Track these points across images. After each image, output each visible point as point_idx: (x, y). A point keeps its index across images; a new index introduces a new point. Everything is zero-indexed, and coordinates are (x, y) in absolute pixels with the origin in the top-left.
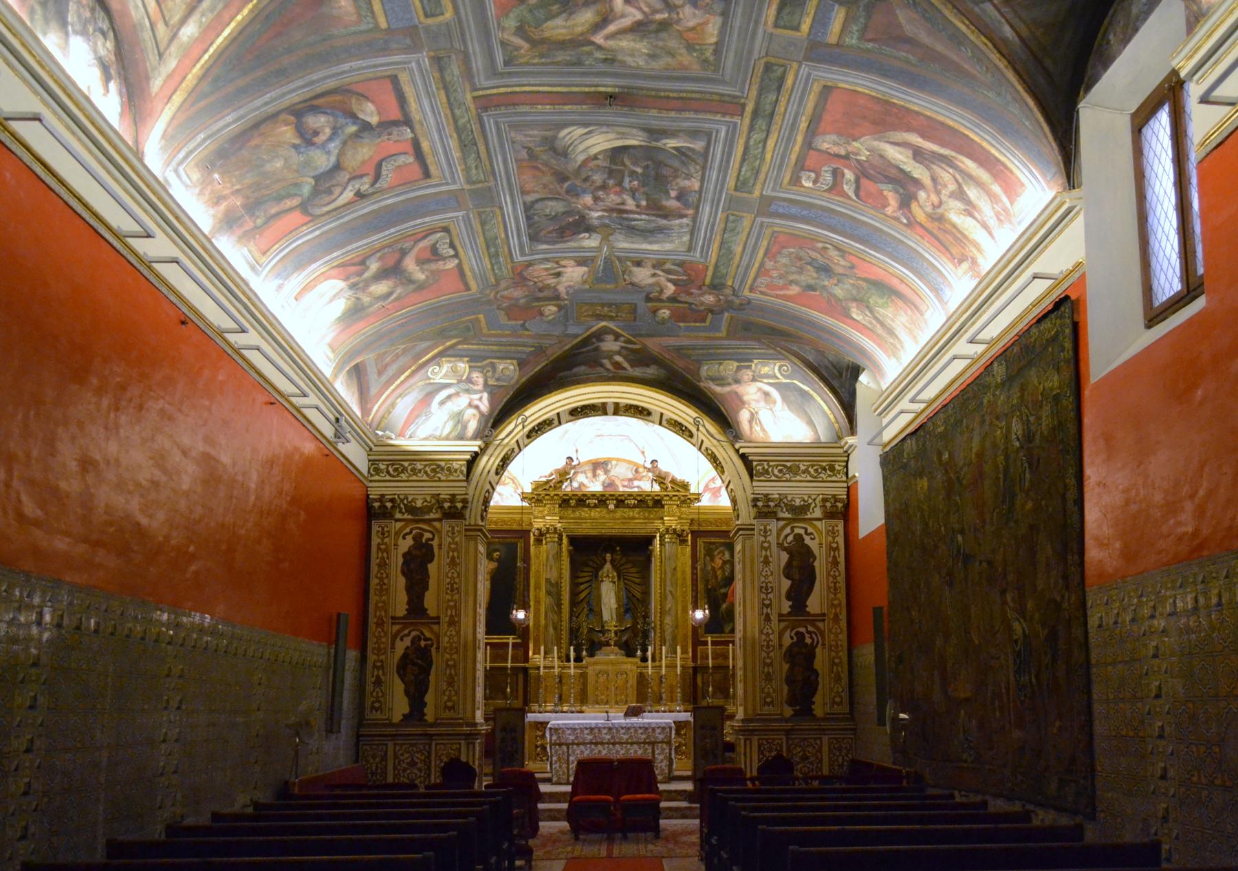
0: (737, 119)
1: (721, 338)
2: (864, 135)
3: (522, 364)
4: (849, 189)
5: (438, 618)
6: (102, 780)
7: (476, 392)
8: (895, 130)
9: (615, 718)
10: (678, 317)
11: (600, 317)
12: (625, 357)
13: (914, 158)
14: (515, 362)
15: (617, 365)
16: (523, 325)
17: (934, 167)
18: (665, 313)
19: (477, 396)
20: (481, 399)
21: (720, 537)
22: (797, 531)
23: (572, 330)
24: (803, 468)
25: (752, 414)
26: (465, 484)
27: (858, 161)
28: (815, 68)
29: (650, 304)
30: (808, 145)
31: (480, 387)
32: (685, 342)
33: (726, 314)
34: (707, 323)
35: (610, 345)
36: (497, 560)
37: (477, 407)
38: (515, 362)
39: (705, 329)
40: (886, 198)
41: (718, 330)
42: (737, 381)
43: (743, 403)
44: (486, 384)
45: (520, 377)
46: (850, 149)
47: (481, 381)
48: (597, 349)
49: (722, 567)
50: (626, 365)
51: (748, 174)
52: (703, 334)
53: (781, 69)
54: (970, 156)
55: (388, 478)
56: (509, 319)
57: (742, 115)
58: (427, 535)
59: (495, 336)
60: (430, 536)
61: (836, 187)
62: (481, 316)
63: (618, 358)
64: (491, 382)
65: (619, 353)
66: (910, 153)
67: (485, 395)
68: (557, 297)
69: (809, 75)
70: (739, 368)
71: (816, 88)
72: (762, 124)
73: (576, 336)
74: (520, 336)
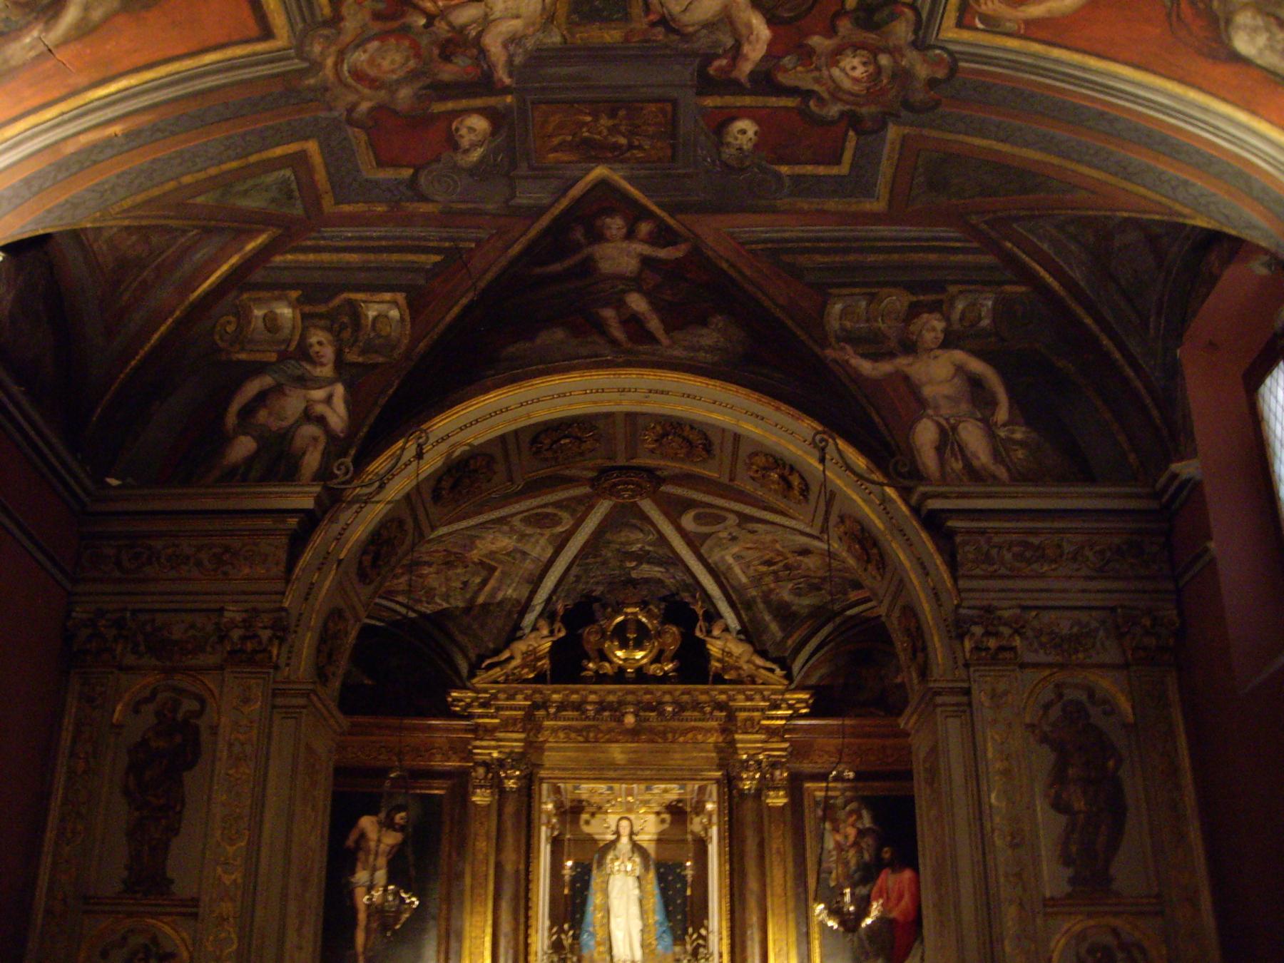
1: (876, 218)
3: (417, 304)
5: (195, 902)
7: (319, 383)
9: (820, 789)
10: (777, 141)
11: (593, 151)
12: (655, 305)
14: (400, 297)
15: (633, 323)
16: (413, 183)
18: (744, 131)
19: (319, 394)
20: (329, 400)
22: (1070, 694)
23: (527, 196)
24: (1068, 548)
25: (942, 431)
26: (279, 586)
29: (710, 102)
31: (327, 371)
32: (793, 231)
33: (893, 132)
34: (844, 169)
35: (619, 255)
36: (402, 829)
37: (321, 420)
38: (400, 297)
39: (838, 187)
41: (867, 191)
42: (910, 347)
43: (922, 403)
44: (339, 363)
45: (415, 341)
47: (328, 353)
48: (588, 267)
49: (855, 844)
50: (654, 324)
52: (832, 205)
55: (117, 574)
56: (381, 164)
58: (189, 705)
59: (353, 220)
60: (195, 705)
62: (312, 146)
63: (637, 303)
64: (352, 357)
65: (636, 283)
67: (339, 390)
68: (484, 83)
70: (914, 311)
73: (540, 211)
74: (409, 220)
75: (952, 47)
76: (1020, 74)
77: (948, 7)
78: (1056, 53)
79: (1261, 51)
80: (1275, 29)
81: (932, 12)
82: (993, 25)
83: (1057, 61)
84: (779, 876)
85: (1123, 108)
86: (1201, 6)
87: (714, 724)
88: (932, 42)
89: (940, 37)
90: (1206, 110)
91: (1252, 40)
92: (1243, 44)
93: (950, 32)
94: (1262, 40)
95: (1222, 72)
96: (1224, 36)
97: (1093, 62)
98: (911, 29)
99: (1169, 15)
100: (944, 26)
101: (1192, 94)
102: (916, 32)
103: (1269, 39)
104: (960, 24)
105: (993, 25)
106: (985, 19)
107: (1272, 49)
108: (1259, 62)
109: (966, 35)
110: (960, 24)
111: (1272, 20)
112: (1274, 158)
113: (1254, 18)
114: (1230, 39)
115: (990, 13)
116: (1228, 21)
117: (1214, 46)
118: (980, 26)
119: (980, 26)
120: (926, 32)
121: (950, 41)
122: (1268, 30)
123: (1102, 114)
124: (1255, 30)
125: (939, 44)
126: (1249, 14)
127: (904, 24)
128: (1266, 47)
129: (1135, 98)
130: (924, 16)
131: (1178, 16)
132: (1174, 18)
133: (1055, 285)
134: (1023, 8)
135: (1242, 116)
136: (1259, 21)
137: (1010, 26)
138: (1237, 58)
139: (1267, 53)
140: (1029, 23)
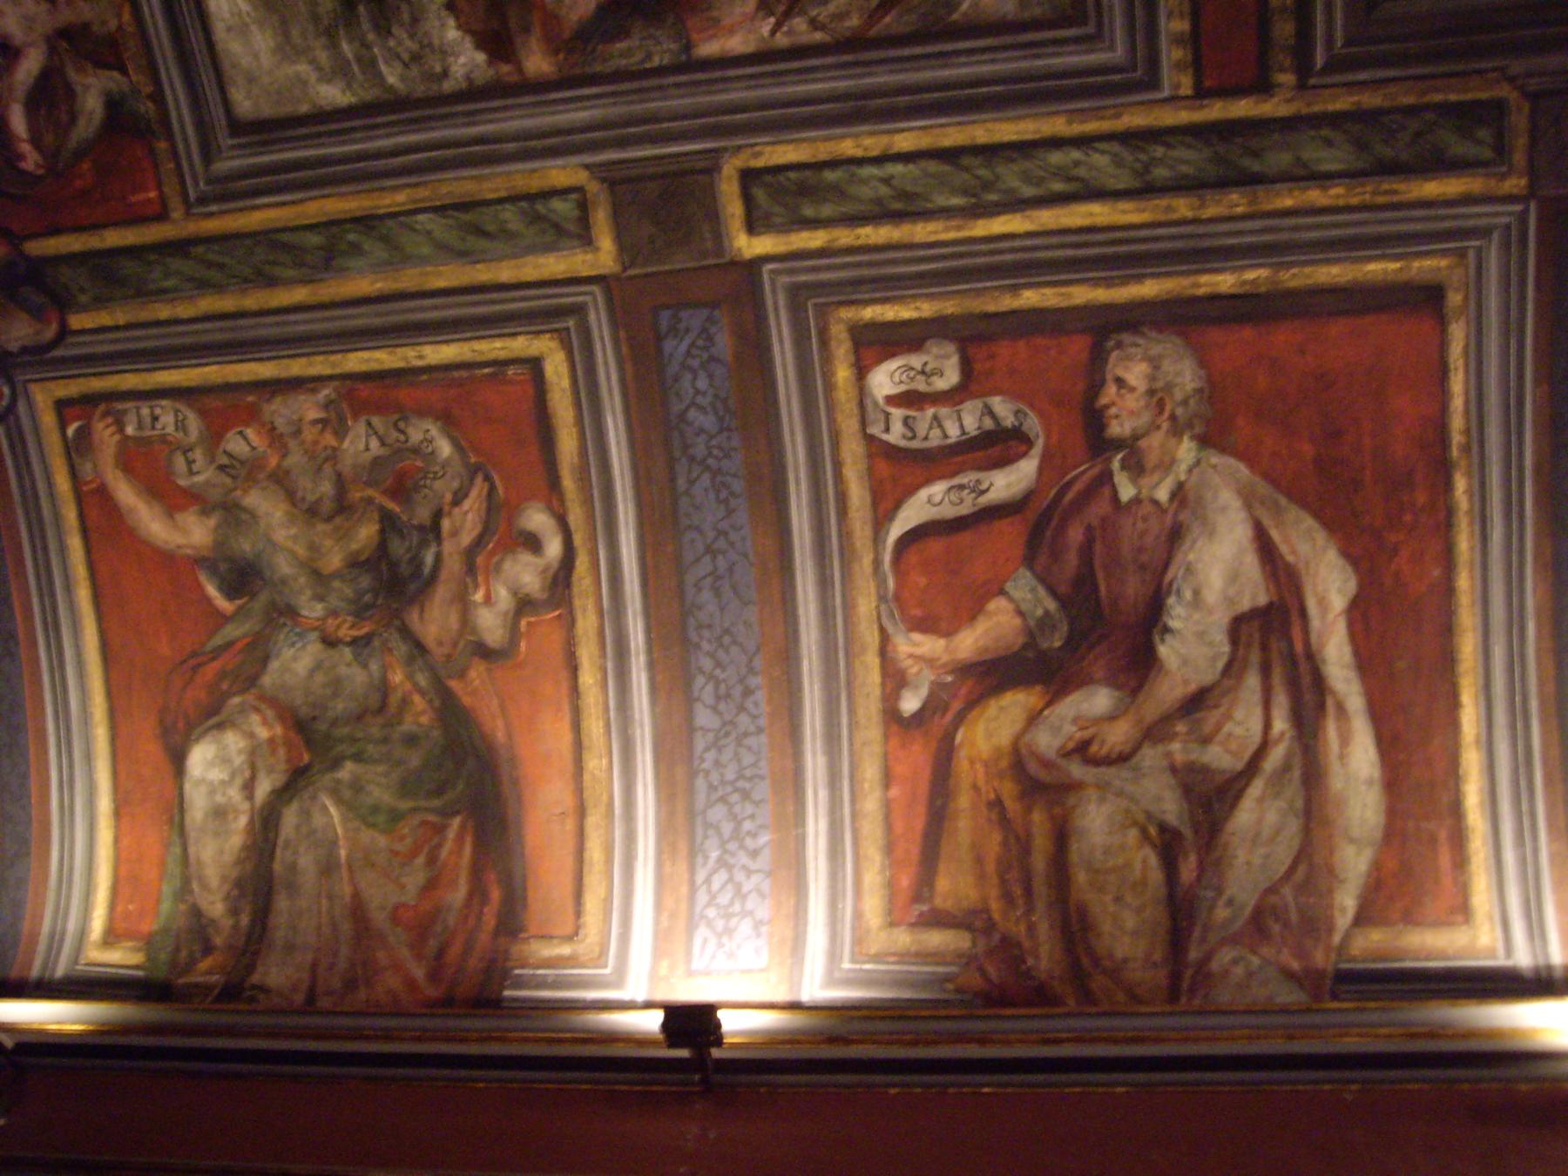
0: (1176, 78)
2: (1247, 456)
4: (929, 502)
6: (697, 1077)
8: (1329, 525)
13: (1237, 626)
17: (1253, 681)
21: (534, 149)
27: (1106, 478)
28: (1513, 240)
30: (1108, 327)
40: (973, 610)
46: (1154, 443)
51: (866, 192)
53: (1487, 154)
54: (1388, 744)
57: (1202, 94)
61: (900, 469)
66: (1255, 592)
69: (1485, 233)
71: (1426, 266)
72: (1189, 159)
75: (22, 408)
76: (20, 511)
77: (81, 380)
78: (75, 543)
79: (202, 781)
80: (239, 781)
81: (63, 361)
82: (79, 448)
83: (63, 550)
84: (1255, 657)
85: (37, 660)
86: (225, 686)
87: (457, 895)
88: (20, 378)
89: (33, 387)
90: (89, 757)
91: (211, 764)
92: (202, 759)
93: (44, 396)
94: (217, 775)
95: (151, 749)
96: (198, 731)
97: (83, 594)
98: (27, 342)
99: (194, 654)
100: (51, 385)
101: (101, 734)
102: (25, 350)
103: (223, 782)
104: (62, 405)
105: (79, 448)
106: (84, 434)
107: (212, 792)
108: (187, 787)
109: (48, 419)
110: (62, 405)
111: (247, 774)
112: (71, 869)
113: (240, 752)
114: (197, 740)
115: (96, 437)
116: (220, 726)
117: (181, 725)
118: (70, 431)
119: (70, 431)
120: (30, 364)
121: (31, 404)
122: (233, 775)
123: (12, 636)
124: (224, 760)
125: (20, 388)
126: (242, 744)
127: (31, 331)
128: (211, 783)
129: (59, 665)
130: (58, 352)
131: (199, 665)
132: (192, 662)
133: (1457, 423)
134: (119, 474)
135: (105, 804)
136: (238, 760)
137: (87, 469)
138: (178, 760)
139: (203, 789)
140: (103, 494)
